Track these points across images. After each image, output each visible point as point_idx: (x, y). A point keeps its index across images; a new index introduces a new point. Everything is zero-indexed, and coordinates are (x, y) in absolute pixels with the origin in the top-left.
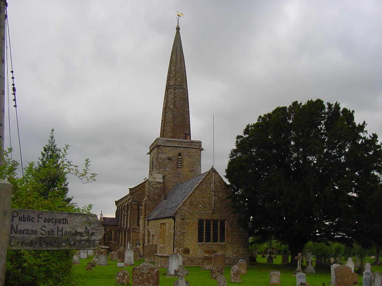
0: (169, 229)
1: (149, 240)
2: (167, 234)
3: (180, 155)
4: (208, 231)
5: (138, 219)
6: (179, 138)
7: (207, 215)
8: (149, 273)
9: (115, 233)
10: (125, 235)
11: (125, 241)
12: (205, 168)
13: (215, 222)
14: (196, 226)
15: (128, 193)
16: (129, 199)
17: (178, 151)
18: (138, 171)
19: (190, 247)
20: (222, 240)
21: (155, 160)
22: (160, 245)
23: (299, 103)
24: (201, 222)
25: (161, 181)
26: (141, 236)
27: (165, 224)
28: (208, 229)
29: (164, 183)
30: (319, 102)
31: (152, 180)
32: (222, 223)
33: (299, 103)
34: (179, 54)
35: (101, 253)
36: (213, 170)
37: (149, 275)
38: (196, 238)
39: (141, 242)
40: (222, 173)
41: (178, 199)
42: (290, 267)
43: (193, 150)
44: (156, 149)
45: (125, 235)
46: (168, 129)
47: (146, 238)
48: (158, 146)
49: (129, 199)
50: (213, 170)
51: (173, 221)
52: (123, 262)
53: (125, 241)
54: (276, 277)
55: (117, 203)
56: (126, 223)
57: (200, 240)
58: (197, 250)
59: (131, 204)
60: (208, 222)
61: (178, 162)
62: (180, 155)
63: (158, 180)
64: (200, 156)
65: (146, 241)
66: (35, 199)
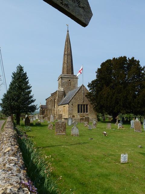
0: (67, 108)
1: (59, 113)
2: (66, 110)
3: (70, 80)
4: (82, 109)
5: (55, 105)
6: (69, 74)
7: (81, 103)
8: (62, 124)
9: (46, 111)
10: (50, 111)
11: (50, 114)
12: (79, 85)
13: (84, 105)
14: (77, 107)
15: (51, 96)
16: (51, 98)
17: (69, 79)
18: (54, 86)
19: (75, 115)
20: (87, 112)
21: (60, 82)
22: (63, 114)
23: (116, 58)
24: (79, 105)
25: (63, 90)
26: (56, 111)
27: (65, 106)
28: (84, 107)
29: (64, 91)
30: (125, 57)
31: (60, 90)
32: (87, 105)
33: (116, 58)
34: (68, 41)
35: (41, 118)
36: (83, 86)
37: (62, 125)
38: (77, 111)
39: (56, 114)
40: (86, 86)
41: (70, 94)
42: (114, 121)
43: (75, 79)
44: (61, 79)
45: (50, 111)
46: (65, 71)
47: (58, 112)
48: (61, 77)
49: (51, 98)
50: (83, 86)
51: (68, 105)
52: (50, 121)
53: (50, 114)
54: (109, 126)
55: (46, 99)
56: (50, 107)
57: (79, 112)
58: (78, 116)
59: (52, 100)
60: (81, 105)
61: (69, 83)
62: (70, 80)
63: (61, 90)
64: (77, 81)
65: (58, 113)
66: (113, 187)
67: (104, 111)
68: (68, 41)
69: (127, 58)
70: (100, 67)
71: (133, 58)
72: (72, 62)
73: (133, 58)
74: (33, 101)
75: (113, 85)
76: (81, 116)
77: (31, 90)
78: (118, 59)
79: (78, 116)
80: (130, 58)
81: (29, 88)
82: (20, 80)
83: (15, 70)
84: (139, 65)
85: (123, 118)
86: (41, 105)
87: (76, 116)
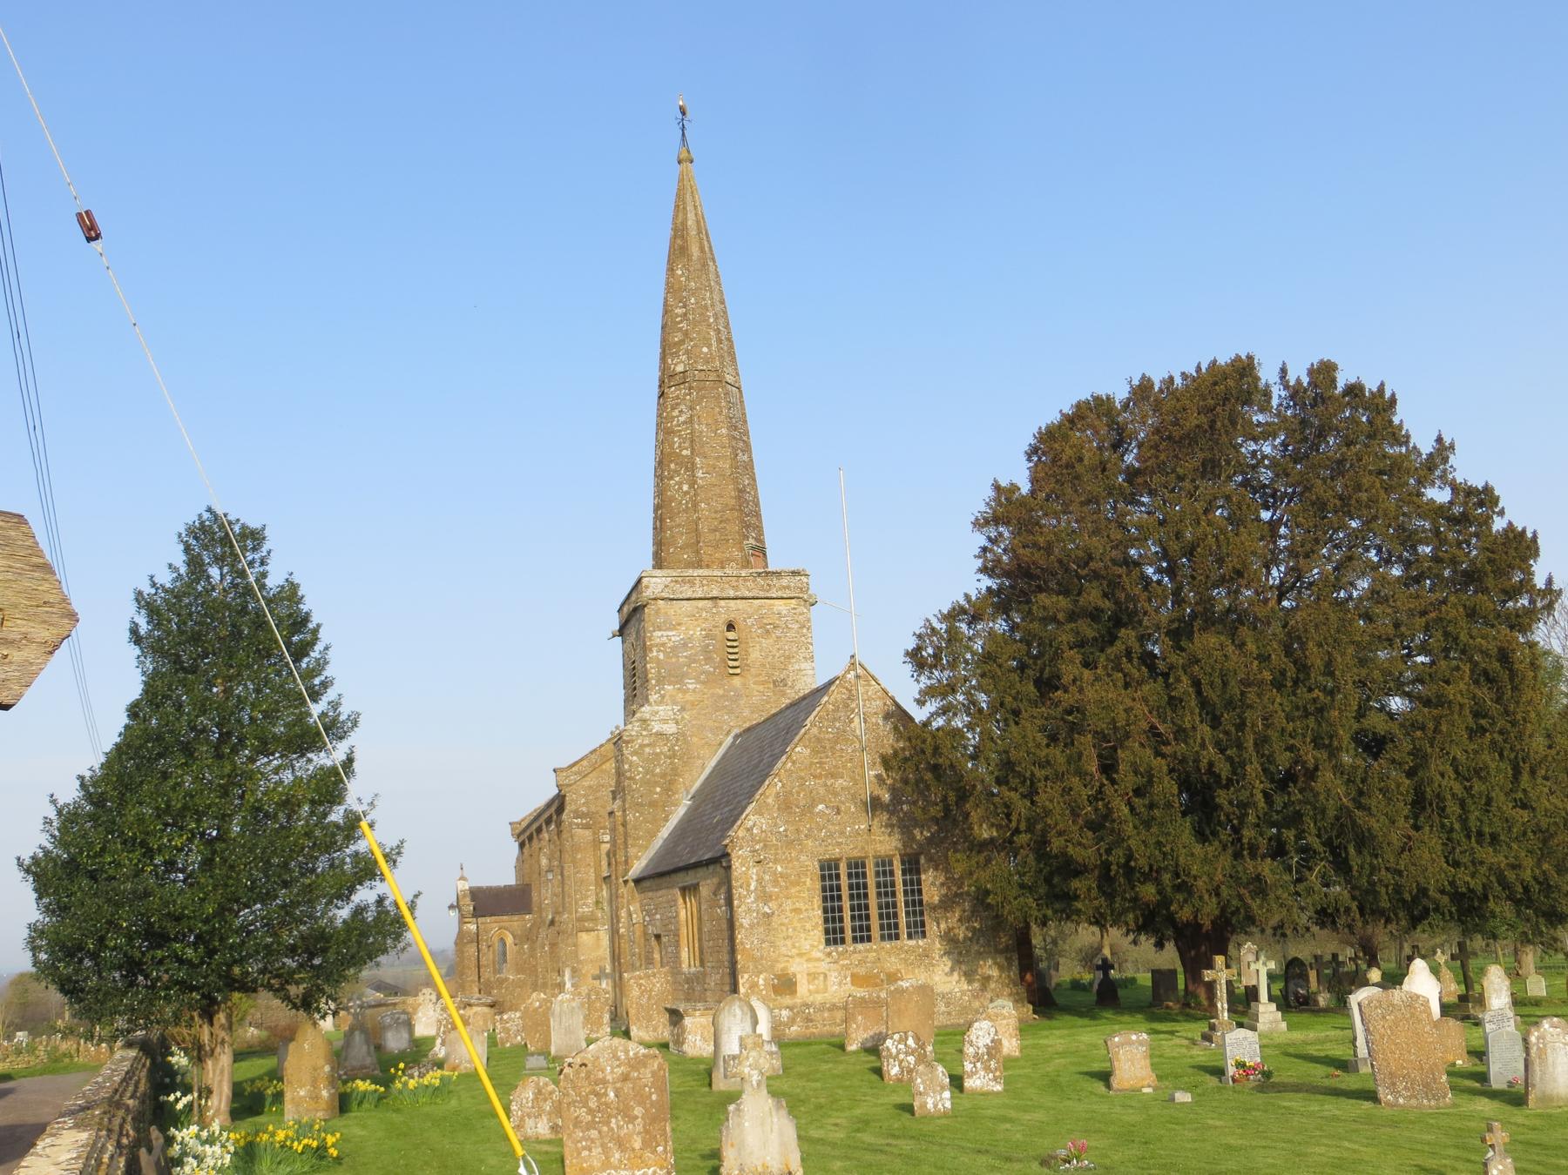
19: (798, 968)
24: (828, 870)
38: (819, 934)
57: (834, 936)
64: (805, 625)
67: (336, 815)
68: (686, 248)
69: (1267, 375)
70: (1020, 476)
71: (1324, 372)
72: (747, 449)
73: (1324, 372)
74: (367, 870)
75: (1264, 857)
76: (862, 971)
77: (349, 762)
78: (1178, 381)
79: (833, 977)
80: (1299, 373)
81: (335, 727)
82: (228, 650)
83: (161, 561)
84: (1398, 436)
85: (1335, 569)
86: (464, 886)
87: (812, 976)
